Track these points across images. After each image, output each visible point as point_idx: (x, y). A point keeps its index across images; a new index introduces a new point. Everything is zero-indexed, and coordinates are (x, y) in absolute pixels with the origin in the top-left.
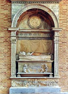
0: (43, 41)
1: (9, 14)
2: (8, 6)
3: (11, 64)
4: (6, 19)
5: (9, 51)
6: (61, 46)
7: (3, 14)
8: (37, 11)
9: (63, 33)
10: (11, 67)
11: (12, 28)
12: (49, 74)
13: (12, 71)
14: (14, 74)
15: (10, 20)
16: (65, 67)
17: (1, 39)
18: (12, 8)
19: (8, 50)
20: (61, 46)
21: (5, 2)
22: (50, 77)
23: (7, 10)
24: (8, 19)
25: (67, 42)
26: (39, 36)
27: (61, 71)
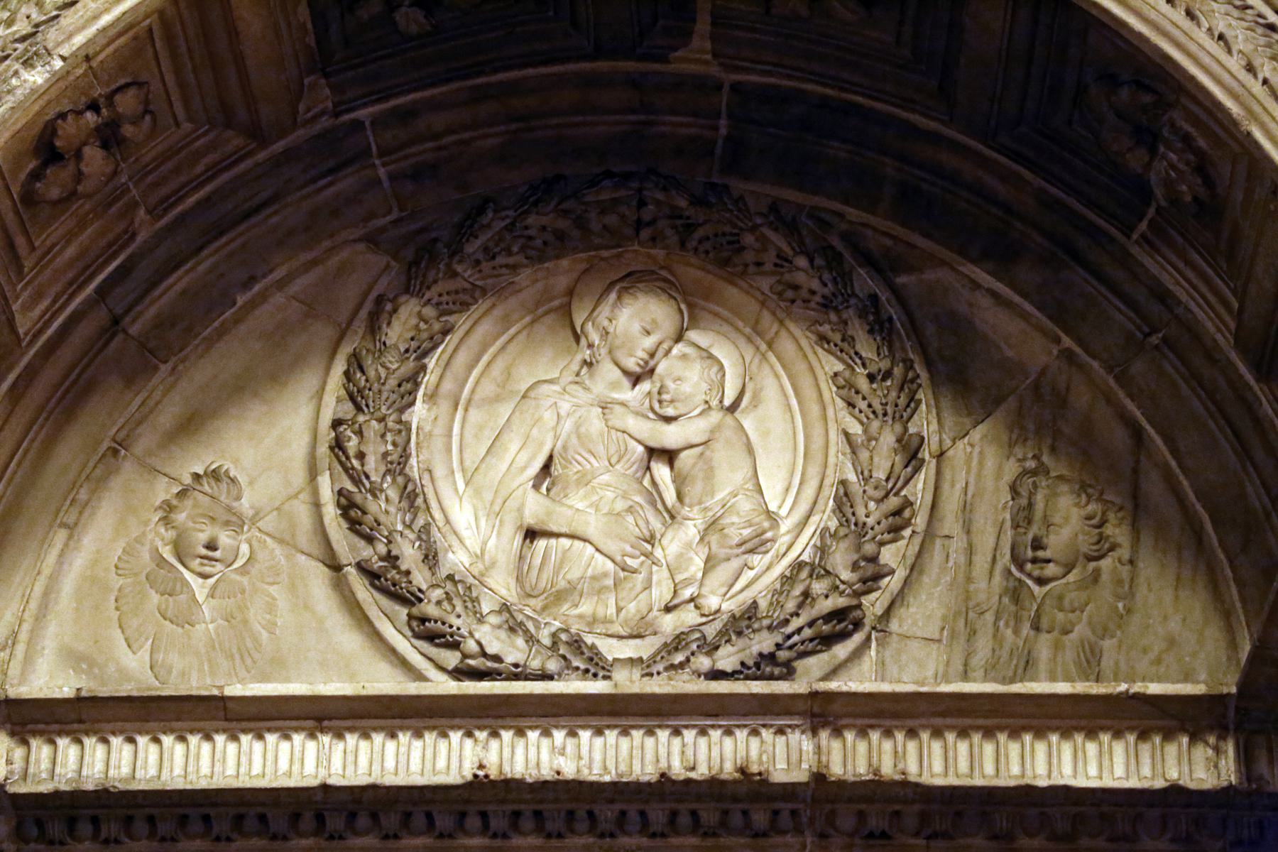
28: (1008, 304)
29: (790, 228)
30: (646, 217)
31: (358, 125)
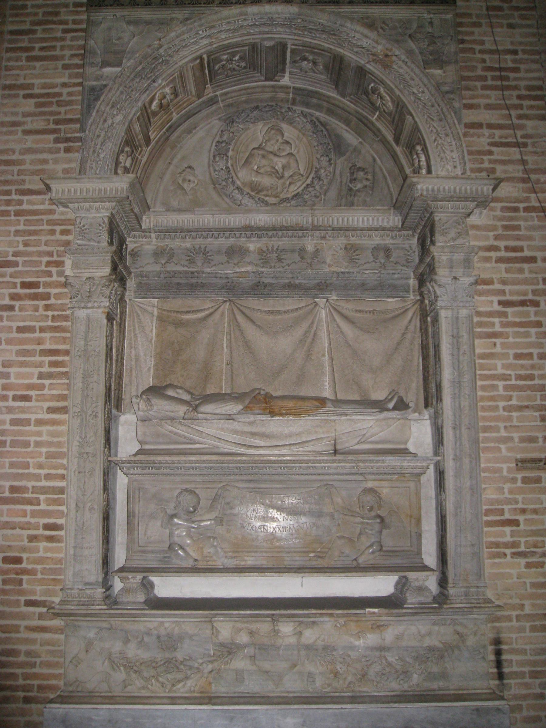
4: (39, 124)
6: (494, 335)
7: (22, 87)
8: (286, 80)
11: (68, 451)
20: (494, 335)
24: (57, 122)
25: (539, 255)
27: (506, 545)
28: (349, 132)
29: (305, 116)
30: (272, 147)
31: (217, 96)
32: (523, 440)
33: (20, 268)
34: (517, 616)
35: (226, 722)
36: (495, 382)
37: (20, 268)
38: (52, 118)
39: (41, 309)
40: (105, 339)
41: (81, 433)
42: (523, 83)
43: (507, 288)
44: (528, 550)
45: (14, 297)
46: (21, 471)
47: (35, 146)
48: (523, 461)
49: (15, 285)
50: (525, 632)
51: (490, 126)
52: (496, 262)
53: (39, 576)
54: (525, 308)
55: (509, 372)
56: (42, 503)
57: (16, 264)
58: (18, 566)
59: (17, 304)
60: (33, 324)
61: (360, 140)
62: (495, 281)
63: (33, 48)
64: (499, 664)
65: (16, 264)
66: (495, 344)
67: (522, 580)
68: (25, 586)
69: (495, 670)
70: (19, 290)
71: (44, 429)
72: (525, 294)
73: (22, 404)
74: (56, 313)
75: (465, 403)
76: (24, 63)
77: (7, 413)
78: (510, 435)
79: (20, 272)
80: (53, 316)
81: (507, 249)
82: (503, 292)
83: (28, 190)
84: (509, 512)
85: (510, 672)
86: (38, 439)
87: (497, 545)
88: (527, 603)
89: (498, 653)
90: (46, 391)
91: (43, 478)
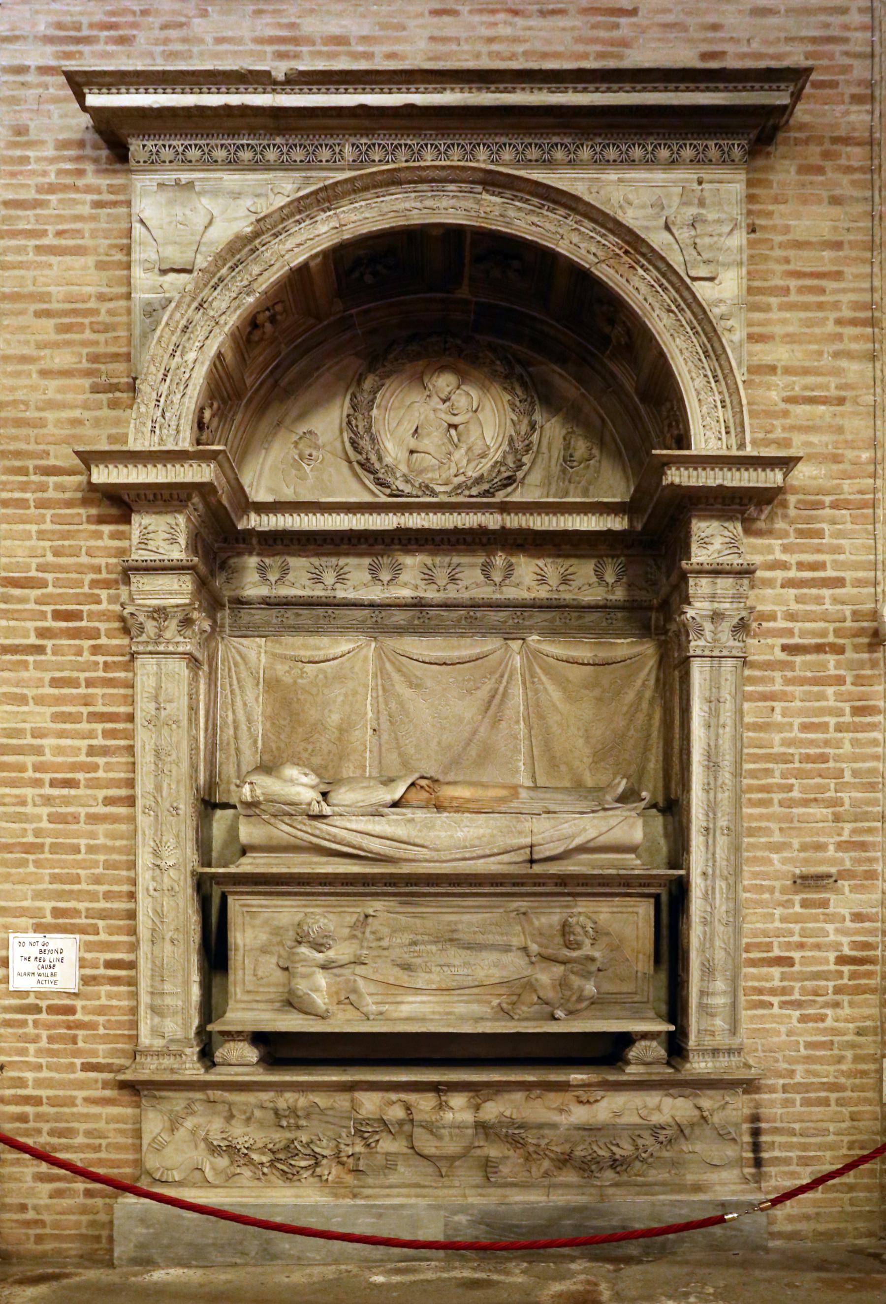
0: (554, 648)
1: (101, 298)
2: (86, 210)
3: (132, 915)
4: (63, 359)
5: (105, 751)
7: (33, 297)
8: (464, 292)
9: (801, 533)
10: (134, 947)
12: (626, 1040)
13: (145, 999)
14: (172, 1027)
15: (118, 372)
16: (818, 947)
17: (6, 599)
18: (137, 227)
19: (91, 735)
21: (52, 160)
22: (633, 1071)
23: (79, 251)
26: (486, 593)
27: (773, 992)
32: (804, 848)
33: (50, 589)
34: (784, 1086)
35: (373, 1220)
36: (770, 766)
37: (50, 589)
38: (85, 351)
39: (86, 654)
40: (186, 698)
41: (155, 834)
42: (846, 298)
43: (797, 626)
44: (803, 998)
45: (42, 633)
46: (67, 887)
47: (59, 397)
48: (804, 877)
49: (43, 616)
50: (795, 1106)
51: (788, 371)
52: (783, 586)
53: (102, 1031)
54: (822, 657)
55: (791, 751)
56: (101, 931)
57: (43, 584)
58: (71, 1018)
59: (49, 643)
60: (75, 674)
61: (583, 390)
62: (779, 614)
63: (44, 233)
64: (756, 1147)
65: (43, 584)
66: (773, 709)
67: (792, 1038)
68: (81, 1044)
69: (750, 1155)
70: (50, 623)
71: (101, 828)
72: (823, 634)
73: (65, 791)
74: (109, 659)
75: (724, 797)
76: (31, 256)
77: (44, 805)
78: (786, 840)
79: (50, 595)
80: (106, 663)
81: (801, 566)
82: (790, 632)
83: (54, 466)
84: (779, 947)
85: (771, 1158)
86: (92, 842)
87: (760, 991)
88: (800, 1068)
89: (756, 1133)
90: (101, 774)
91: (101, 896)
